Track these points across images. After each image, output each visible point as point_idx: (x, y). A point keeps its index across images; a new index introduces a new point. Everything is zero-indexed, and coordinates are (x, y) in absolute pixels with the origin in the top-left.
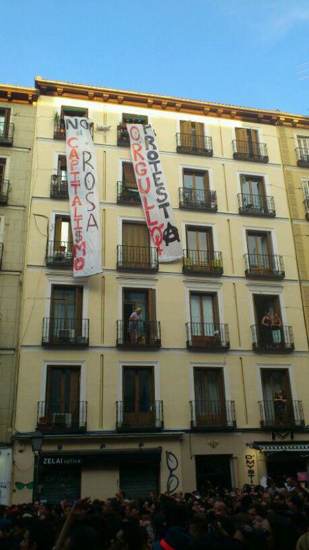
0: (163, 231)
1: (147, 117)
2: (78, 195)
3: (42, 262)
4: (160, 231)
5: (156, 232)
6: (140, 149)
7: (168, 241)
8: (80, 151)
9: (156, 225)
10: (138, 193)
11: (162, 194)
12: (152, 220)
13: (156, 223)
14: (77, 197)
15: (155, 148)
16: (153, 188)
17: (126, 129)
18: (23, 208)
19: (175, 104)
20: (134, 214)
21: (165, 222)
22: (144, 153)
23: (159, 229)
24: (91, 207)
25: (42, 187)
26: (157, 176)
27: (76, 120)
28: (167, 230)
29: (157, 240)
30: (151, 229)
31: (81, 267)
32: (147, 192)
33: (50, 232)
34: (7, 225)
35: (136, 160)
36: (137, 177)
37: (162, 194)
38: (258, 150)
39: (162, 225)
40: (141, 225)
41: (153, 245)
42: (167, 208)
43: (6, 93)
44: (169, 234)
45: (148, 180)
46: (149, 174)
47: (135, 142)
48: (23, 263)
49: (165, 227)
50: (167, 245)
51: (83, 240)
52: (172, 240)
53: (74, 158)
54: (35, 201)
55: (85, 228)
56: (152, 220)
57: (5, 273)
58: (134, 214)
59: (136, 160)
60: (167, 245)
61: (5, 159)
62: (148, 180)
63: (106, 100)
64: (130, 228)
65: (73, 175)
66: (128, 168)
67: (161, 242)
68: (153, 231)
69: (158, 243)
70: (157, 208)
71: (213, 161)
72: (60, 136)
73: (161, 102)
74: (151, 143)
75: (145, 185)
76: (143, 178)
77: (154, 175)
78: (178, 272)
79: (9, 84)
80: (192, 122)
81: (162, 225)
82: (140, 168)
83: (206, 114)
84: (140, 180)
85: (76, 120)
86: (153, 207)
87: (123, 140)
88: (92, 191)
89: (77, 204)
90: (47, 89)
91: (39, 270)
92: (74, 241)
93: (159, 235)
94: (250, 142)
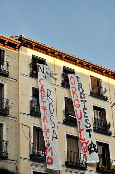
0: (88, 144)
1: (45, 59)
2: (46, 116)
3: (28, 157)
4: (87, 145)
5: (84, 145)
6: (75, 91)
7: (91, 151)
8: (45, 88)
9: (84, 141)
10: (76, 119)
11: (88, 123)
12: (83, 138)
13: (84, 140)
14: (45, 117)
15: (83, 91)
16: (84, 119)
17: (68, 77)
18: (15, 119)
19: (31, 44)
20: (72, 131)
21: (90, 140)
22: (78, 93)
23: (86, 144)
24: (53, 126)
25: (26, 108)
26: (85, 111)
27: (44, 67)
28: (91, 144)
29: (85, 150)
30: (82, 142)
31: (52, 163)
32: (81, 118)
33: (31, 137)
34: (7, 129)
35: (74, 97)
36: (75, 108)
37: (88, 123)
38: (102, 92)
39: (88, 141)
40: (76, 139)
41: (81, 152)
42: (91, 132)
43: (5, 41)
44: (91, 147)
45: (80, 111)
46: (82, 108)
47: (73, 86)
48: (18, 156)
49: (90, 143)
50: (90, 154)
51: (51, 146)
52: (93, 151)
53: (43, 92)
54: (22, 115)
55: (51, 139)
56: (83, 138)
57: (9, 161)
58: (72, 131)
59: (74, 97)
60: (90, 154)
61: (3, 85)
62: (80, 111)
63: (54, 56)
64: (72, 140)
65: (43, 102)
66: (69, 102)
67: (87, 151)
68: (82, 144)
69: (85, 152)
70: (85, 131)
71: (107, 103)
72: (34, 75)
73: (47, 50)
74: (81, 87)
75: (79, 116)
76: (78, 109)
77: (84, 109)
78: (95, 170)
79: (6, 35)
80: (97, 78)
81: (88, 141)
82: (76, 102)
83: (47, 54)
84: (76, 110)
85: (44, 67)
86: (83, 130)
87: (66, 84)
88: (52, 115)
89: (45, 121)
90: (27, 44)
91: (27, 161)
92: (46, 146)
93: (86, 147)
94: (98, 86)
